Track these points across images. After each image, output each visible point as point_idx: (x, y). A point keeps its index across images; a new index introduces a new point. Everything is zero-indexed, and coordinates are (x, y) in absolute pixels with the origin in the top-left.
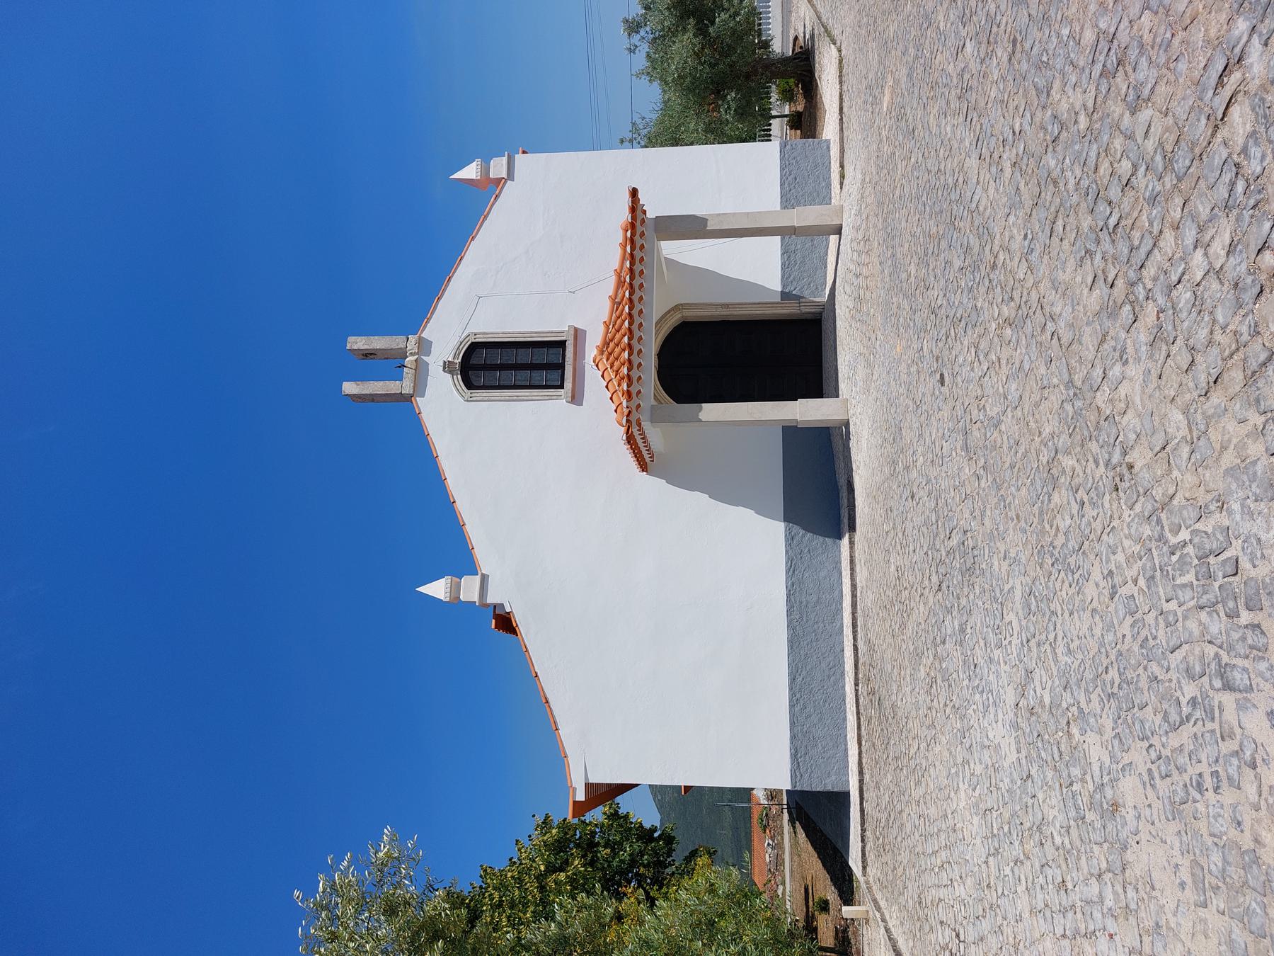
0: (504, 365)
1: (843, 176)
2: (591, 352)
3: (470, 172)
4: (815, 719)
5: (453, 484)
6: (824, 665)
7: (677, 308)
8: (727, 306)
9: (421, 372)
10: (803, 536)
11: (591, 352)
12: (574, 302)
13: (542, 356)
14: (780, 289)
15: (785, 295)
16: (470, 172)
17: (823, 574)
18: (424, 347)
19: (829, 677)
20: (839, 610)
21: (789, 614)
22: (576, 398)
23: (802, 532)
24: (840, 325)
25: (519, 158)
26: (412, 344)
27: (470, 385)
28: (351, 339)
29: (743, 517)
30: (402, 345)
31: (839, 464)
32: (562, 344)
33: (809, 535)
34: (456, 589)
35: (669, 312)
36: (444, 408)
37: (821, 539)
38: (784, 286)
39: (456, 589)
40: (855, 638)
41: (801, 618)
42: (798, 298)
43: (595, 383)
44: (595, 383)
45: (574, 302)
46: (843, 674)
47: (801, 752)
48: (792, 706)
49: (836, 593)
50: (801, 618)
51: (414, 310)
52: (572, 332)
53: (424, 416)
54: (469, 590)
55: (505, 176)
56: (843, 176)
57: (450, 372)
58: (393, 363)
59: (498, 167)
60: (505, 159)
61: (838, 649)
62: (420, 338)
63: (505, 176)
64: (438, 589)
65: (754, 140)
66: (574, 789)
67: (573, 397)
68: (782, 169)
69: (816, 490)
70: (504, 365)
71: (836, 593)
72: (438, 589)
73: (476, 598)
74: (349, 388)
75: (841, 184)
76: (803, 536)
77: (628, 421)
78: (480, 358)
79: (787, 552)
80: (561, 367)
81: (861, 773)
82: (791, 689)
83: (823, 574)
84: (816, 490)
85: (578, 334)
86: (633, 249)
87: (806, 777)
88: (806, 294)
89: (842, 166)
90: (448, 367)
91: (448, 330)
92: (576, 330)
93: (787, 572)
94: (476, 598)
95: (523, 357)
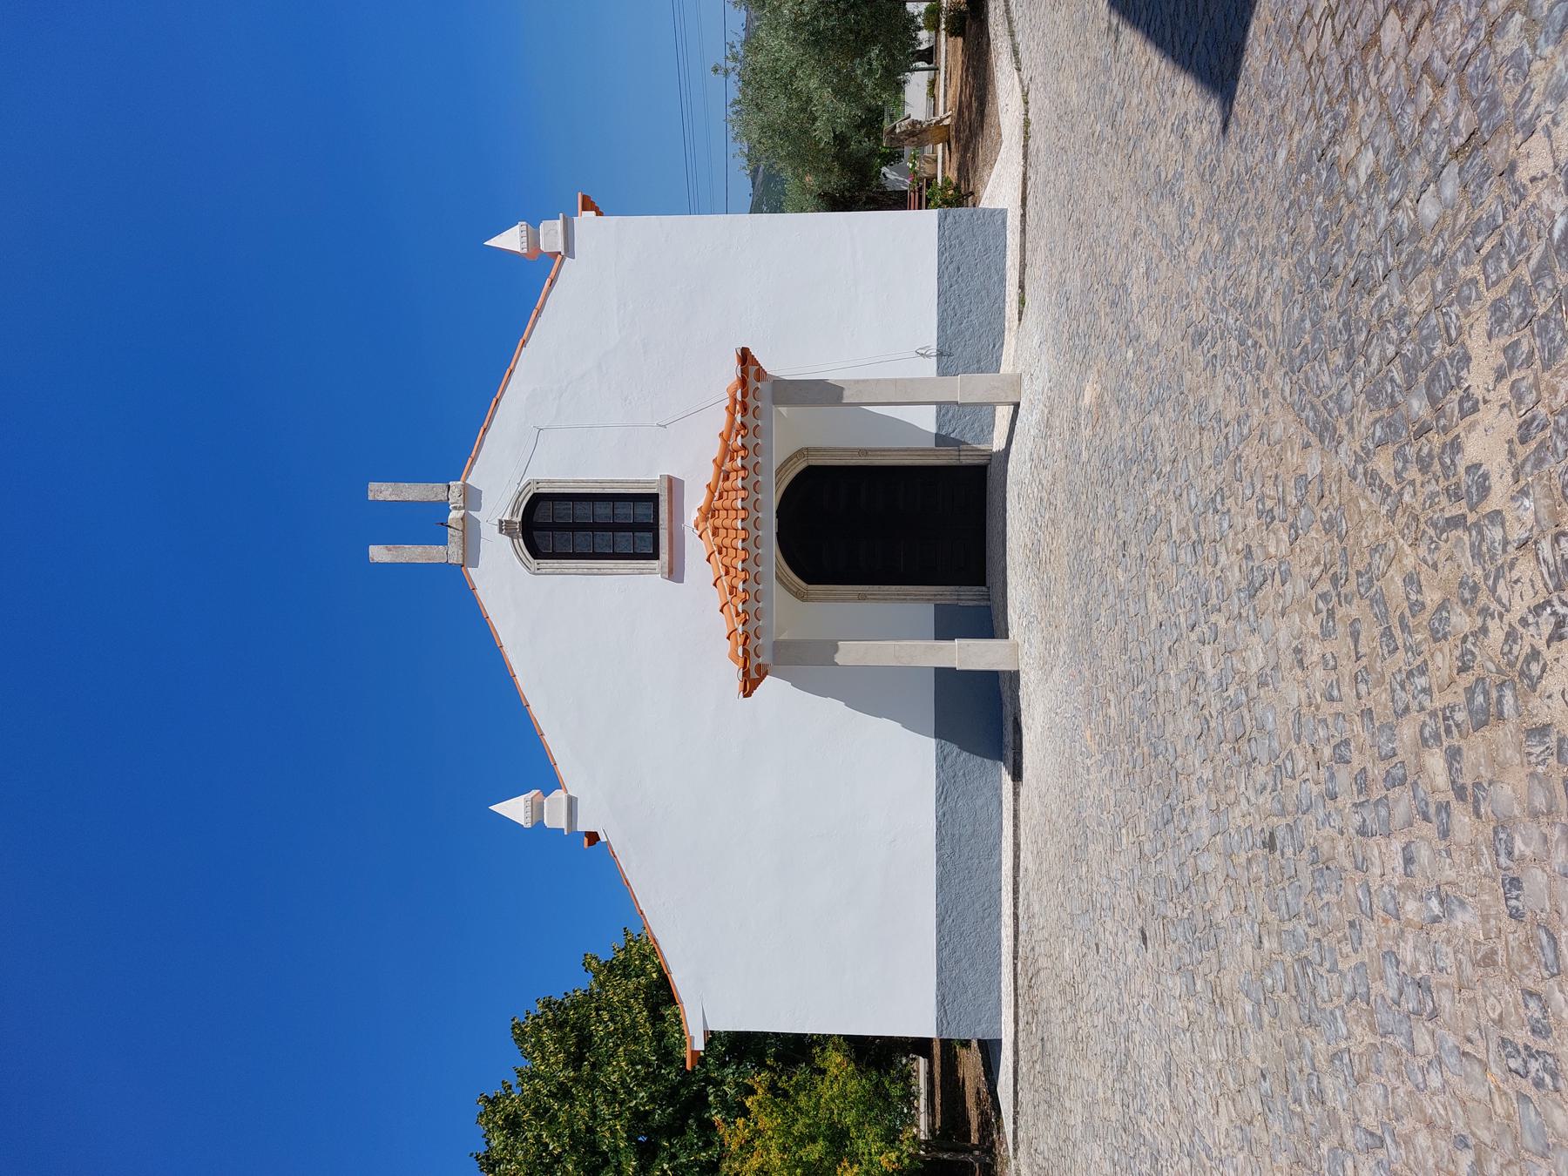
0: (581, 526)
1: (1022, 302)
2: (691, 515)
3: (511, 240)
4: (965, 964)
5: (521, 680)
6: (977, 905)
7: (800, 453)
8: (864, 452)
9: (470, 531)
10: (958, 755)
11: (691, 515)
12: (671, 443)
13: (625, 512)
14: (934, 431)
15: (940, 439)
16: (511, 240)
17: (979, 802)
18: (472, 498)
19: (983, 919)
20: (998, 904)
21: (939, 847)
22: (675, 573)
23: (956, 749)
24: (1012, 544)
25: (585, 221)
26: (455, 497)
27: (536, 552)
28: (373, 486)
29: (888, 729)
30: (442, 497)
31: (1008, 710)
32: (653, 498)
33: (965, 754)
34: (537, 809)
35: (790, 459)
36: (504, 580)
37: (979, 760)
38: (939, 427)
39: (533, 240)
40: (1016, 906)
41: (953, 852)
42: (957, 443)
43: (696, 548)
44: (696, 548)
45: (671, 443)
46: (999, 915)
47: (949, 999)
48: (939, 951)
49: (995, 825)
50: (953, 852)
51: (452, 451)
52: (666, 484)
53: (480, 592)
54: (556, 818)
55: (560, 248)
56: (1022, 302)
57: (509, 534)
58: (427, 523)
59: (551, 235)
60: (559, 224)
61: (994, 889)
62: (466, 487)
63: (560, 248)
64: (515, 809)
65: (904, 207)
66: (692, 1038)
67: (671, 571)
68: (941, 254)
69: (978, 718)
70: (581, 526)
71: (995, 825)
72: (515, 809)
73: (563, 824)
74: (378, 554)
75: (1020, 313)
76: (958, 755)
77: (745, 651)
78: (543, 514)
79: (938, 776)
80: (653, 528)
81: (1016, 1053)
82: (939, 932)
83: (979, 802)
84: (978, 718)
85: (673, 484)
86: (744, 395)
87: (954, 1025)
88: (968, 438)
89: (1022, 287)
90: (506, 527)
91: (502, 472)
92: (670, 480)
93: (938, 800)
94: (563, 824)
95: (603, 512)
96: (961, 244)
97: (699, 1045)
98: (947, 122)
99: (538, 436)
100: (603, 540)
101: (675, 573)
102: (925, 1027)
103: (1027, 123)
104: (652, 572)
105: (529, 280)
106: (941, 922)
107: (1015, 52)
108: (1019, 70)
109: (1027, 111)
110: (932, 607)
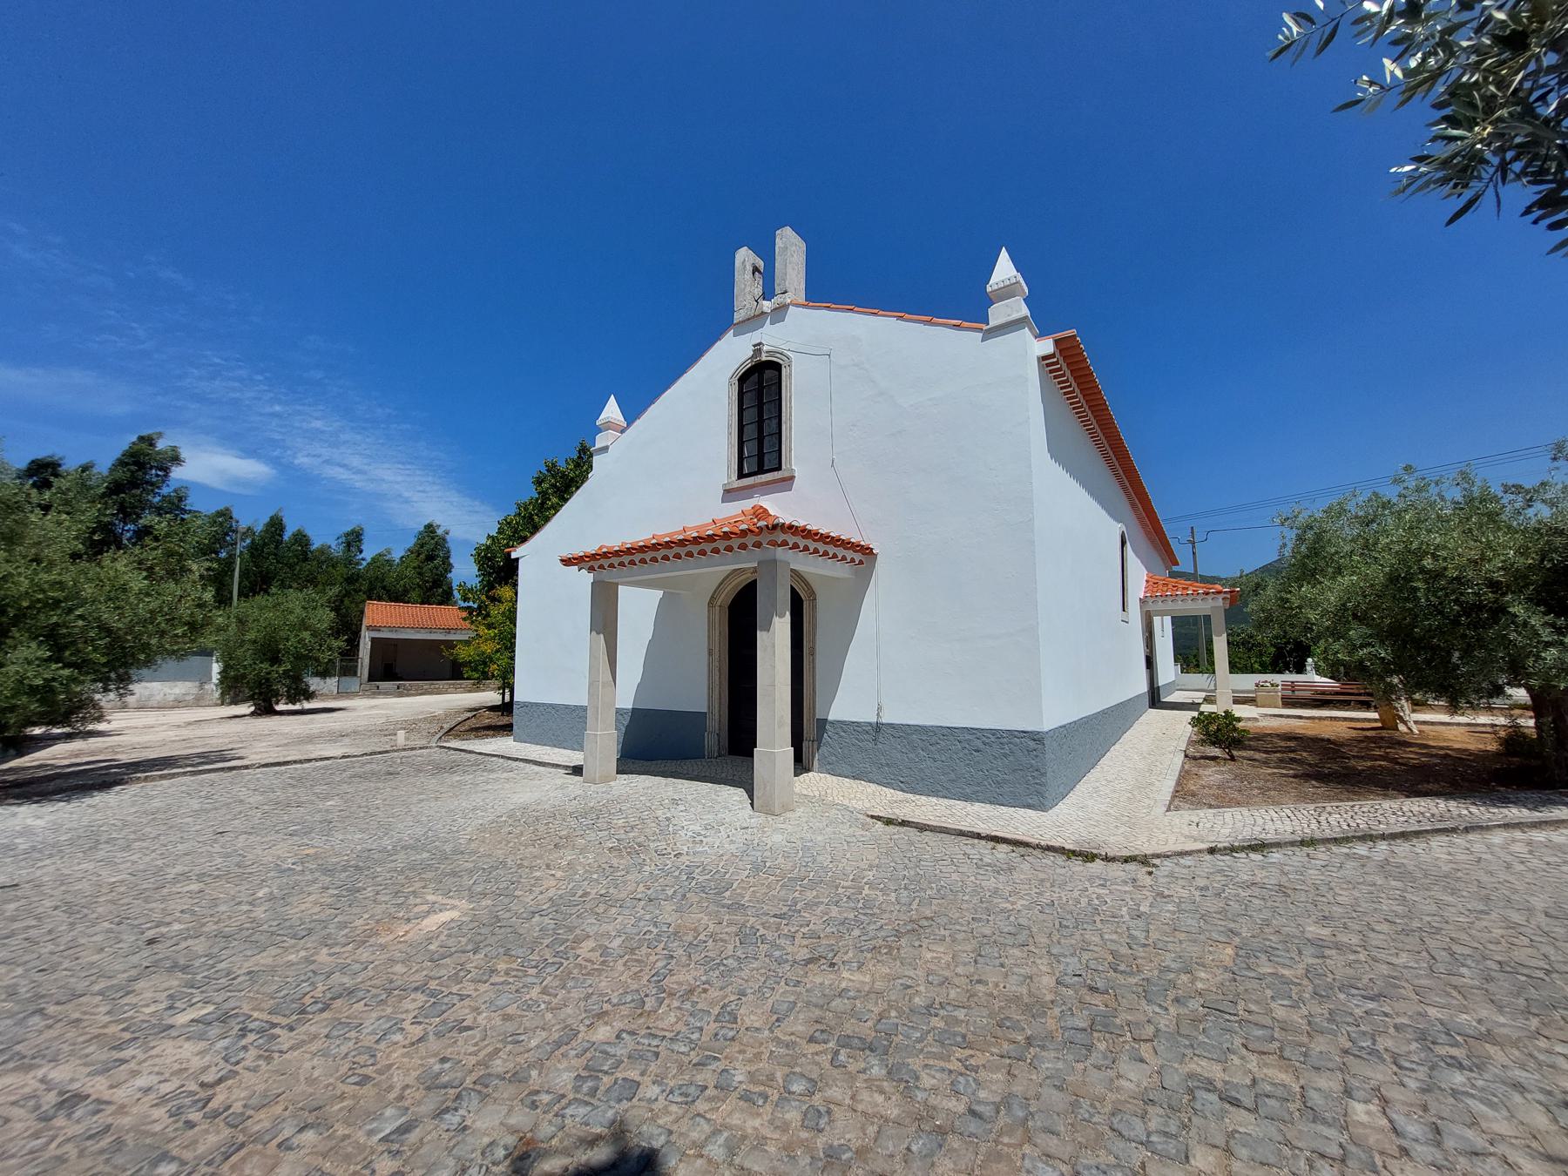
3: (1004, 270)
8: (812, 654)
14: (831, 718)
22: (729, 494)
27: (743, 379)
42: (819, 739)
51: (830, 287)
68: (994, 732)
80: (761, 470)
88: (823, 749)
90: (758, 349)
92: (792, 478)
96: (1005, 755)
97: (514, 556)
98: (1402, 727)
99: (838, 356)
100: (751, 431)
101: (729, 494)
102: (524, 691)
103: (1089, 857)
104: (729, 477)
105: (965, 304)
106: (552, 706)
107: (1260, 847)
108: (1212, 851)
109: (1108, 859)
110: (702, 708)
